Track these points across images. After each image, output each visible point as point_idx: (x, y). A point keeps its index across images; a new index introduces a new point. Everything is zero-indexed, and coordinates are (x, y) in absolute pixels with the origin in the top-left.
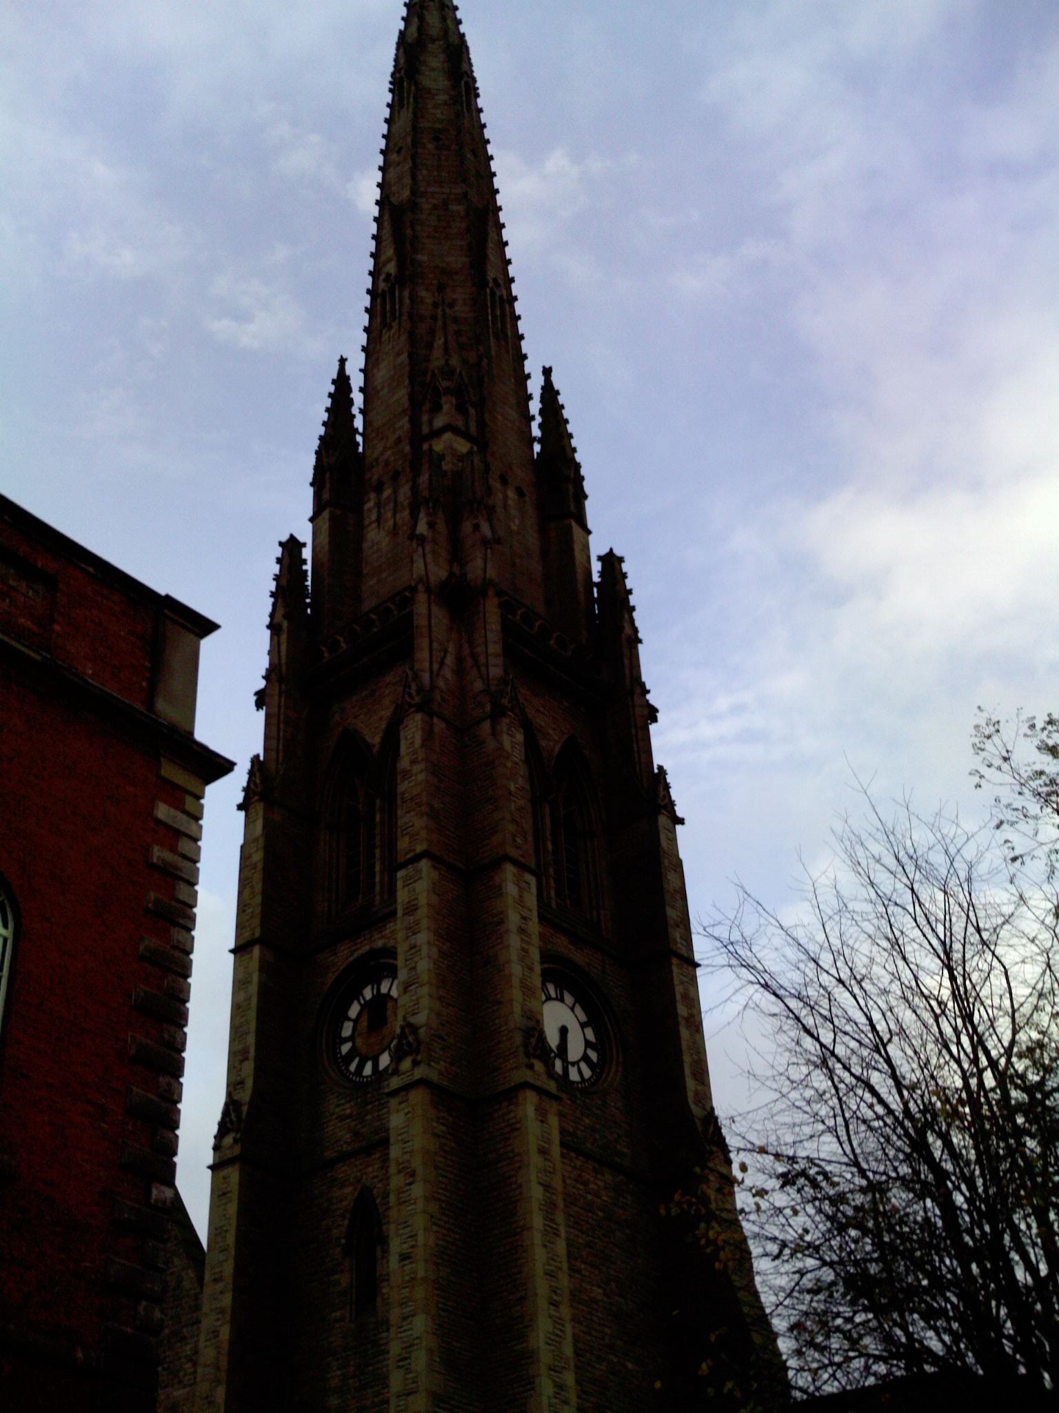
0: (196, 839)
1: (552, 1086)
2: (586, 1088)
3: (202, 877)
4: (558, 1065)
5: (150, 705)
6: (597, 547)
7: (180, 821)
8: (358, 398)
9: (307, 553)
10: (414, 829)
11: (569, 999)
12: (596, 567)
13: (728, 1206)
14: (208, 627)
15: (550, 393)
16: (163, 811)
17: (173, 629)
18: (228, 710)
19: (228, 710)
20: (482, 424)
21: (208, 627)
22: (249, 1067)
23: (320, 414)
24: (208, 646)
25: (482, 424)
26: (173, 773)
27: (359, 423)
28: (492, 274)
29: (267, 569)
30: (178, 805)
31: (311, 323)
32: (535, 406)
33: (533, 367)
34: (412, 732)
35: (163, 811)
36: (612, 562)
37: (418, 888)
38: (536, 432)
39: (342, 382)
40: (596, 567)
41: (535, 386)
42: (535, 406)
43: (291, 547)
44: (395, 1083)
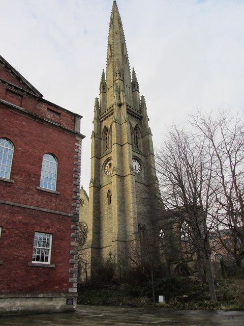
0: (80, 179)
1: (134, 174)
2: (139, 174)
3: (82, 165)
4: (135, 171)
5: (74, 130)
6: (141, 95)
7: (77, 176)
8: (105, 75)
9: (99, 100)
10: (114, 139)
11: (136, 161)
12: (140, 98)
13: (93, 249)
14: (81, 117)
15: (134, 72)
16: (76, 144)
17: (75, 118)
18: (87, 127)
19: (87, 127)
20: (123, 78)
21: (81, 117)
22: (94, 174)
23: (106, 29)
24: (81, 119)
25: (123, 78)
26: (77, 138)
27: (106, 79)
28: (125, 53)
29: (93, 103)
30: (78, 143)
31: (97, 62)
32: (131, 74)
33: (131, 68)
34: (114, 125)
35: (76, 144)
36: (143, 97)
37: (115, 148)
38: (132, 78)
39: (103, 73)
40: (140, 98)
41: (131, 71)
42: (131, 74)
43: (97, 99)
44: (112, 175)
